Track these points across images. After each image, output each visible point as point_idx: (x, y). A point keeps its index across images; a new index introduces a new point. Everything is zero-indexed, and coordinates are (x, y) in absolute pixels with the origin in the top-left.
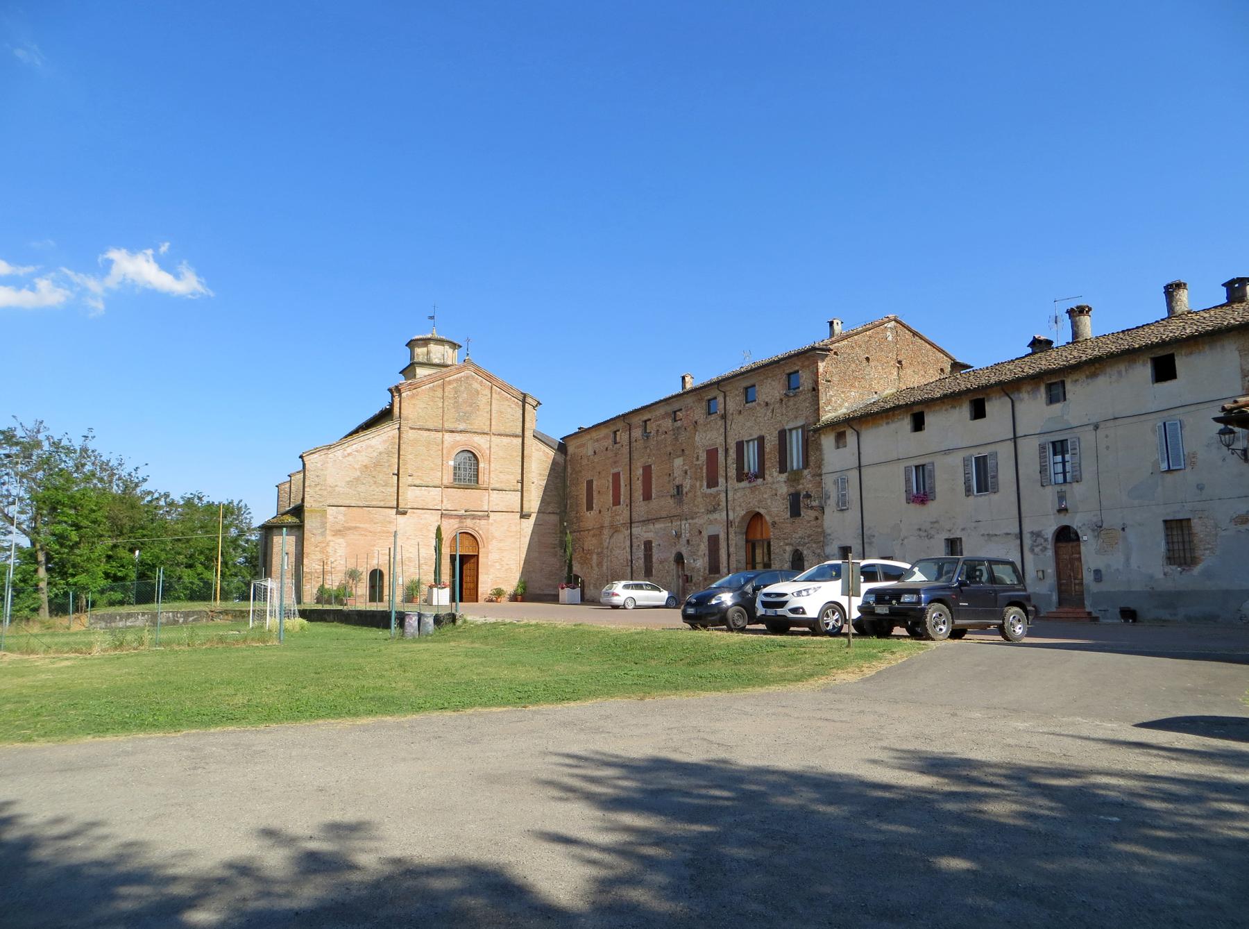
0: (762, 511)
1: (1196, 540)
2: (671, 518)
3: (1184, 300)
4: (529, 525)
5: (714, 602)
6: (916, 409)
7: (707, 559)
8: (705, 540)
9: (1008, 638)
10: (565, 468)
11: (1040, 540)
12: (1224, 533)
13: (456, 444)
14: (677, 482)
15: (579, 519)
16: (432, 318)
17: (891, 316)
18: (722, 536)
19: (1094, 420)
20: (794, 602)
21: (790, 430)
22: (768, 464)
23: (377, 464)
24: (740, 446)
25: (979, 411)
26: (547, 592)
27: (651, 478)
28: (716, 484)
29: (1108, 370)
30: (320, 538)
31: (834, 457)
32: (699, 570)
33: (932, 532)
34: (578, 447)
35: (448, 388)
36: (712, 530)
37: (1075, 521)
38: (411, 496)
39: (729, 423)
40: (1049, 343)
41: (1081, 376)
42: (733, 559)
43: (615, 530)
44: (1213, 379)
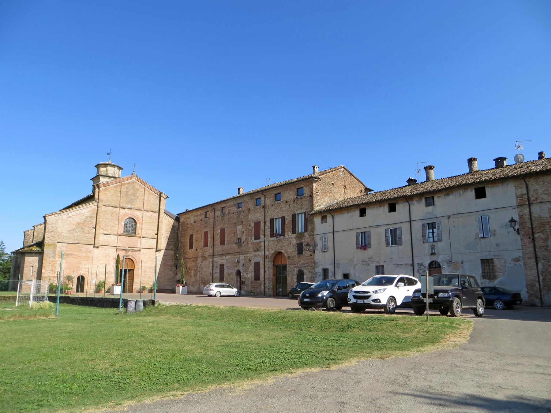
0: (283, 251)
1: (496, 268)
2: (234, 254)
3: (476, 166)
4: (160, 256)
5: (320, 295)
6: (362, 207)
7: (253, 273)
8: (253, 264)
9: (478, 315)
10: (178, 228)
11: (422, 267)
12: (509, 265)
13: (126, 214)
14: (239, 236)
15: (185, 253)
16: (109, 154)
17: (343, 166)
18: (262, 263)
19: (448, 214)
20: (375, 296)
21: (298, 214)
22: (286, 229)
23: (85, 223)
24: (272, 221)
25: (392, 209)
26: (167, 288)
27: (224, 234)
28: (259, 238)
29: (455, 193)
30: (52, 259)
31: (319, 226)
32: (249, 278)
33: (369, 263)
34: (186, 219)
35: (123, 187)
36: (256, 260)
37: (439, 259)
38: (101, 239)
39: (267, 210)
40: (416, 181)
41: (442, 195)
42: (267, 273)
43: (204, 258)
44: (503, 198)
